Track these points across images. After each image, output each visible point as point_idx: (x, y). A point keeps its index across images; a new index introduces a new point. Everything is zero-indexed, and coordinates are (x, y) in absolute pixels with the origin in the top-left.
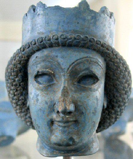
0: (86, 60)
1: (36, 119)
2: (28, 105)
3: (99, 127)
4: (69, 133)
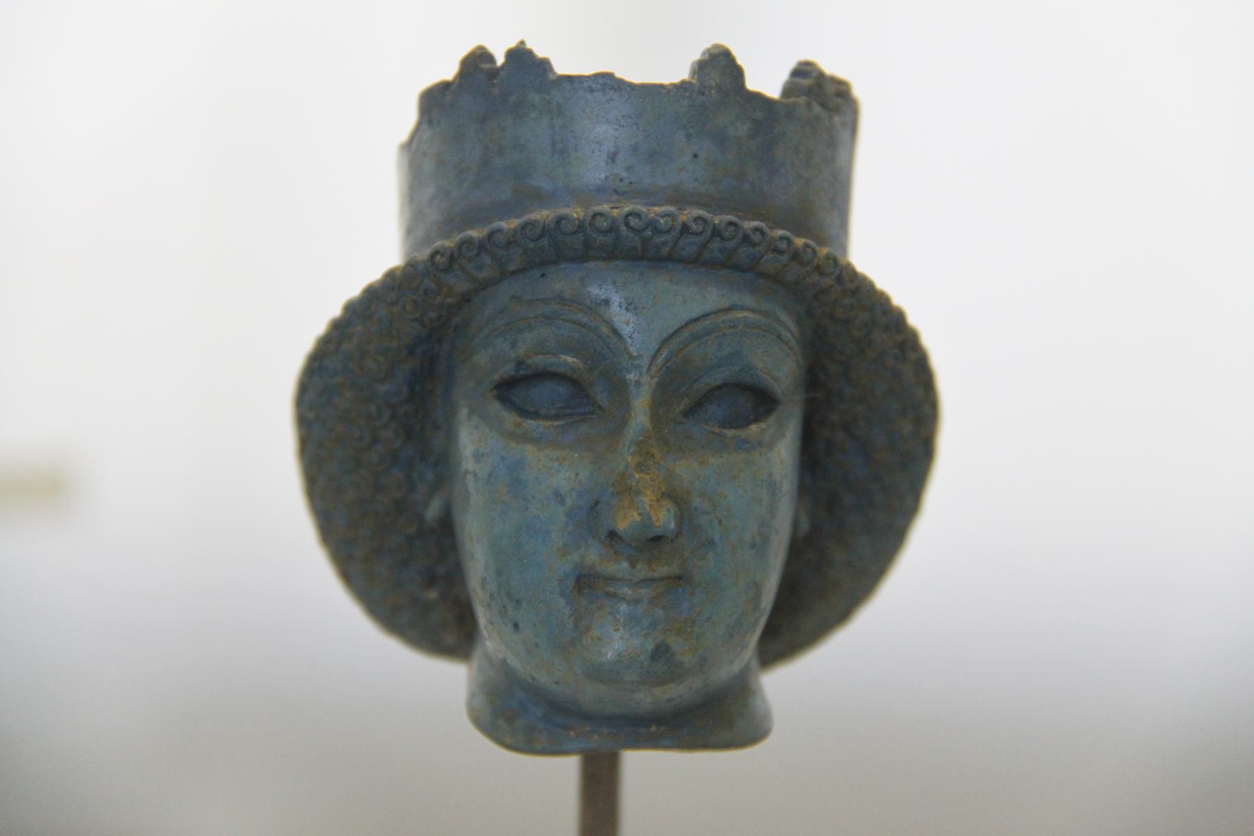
0: (765, 539)
1: (685, 403)
3: (770, 632)
4: (654, 625)
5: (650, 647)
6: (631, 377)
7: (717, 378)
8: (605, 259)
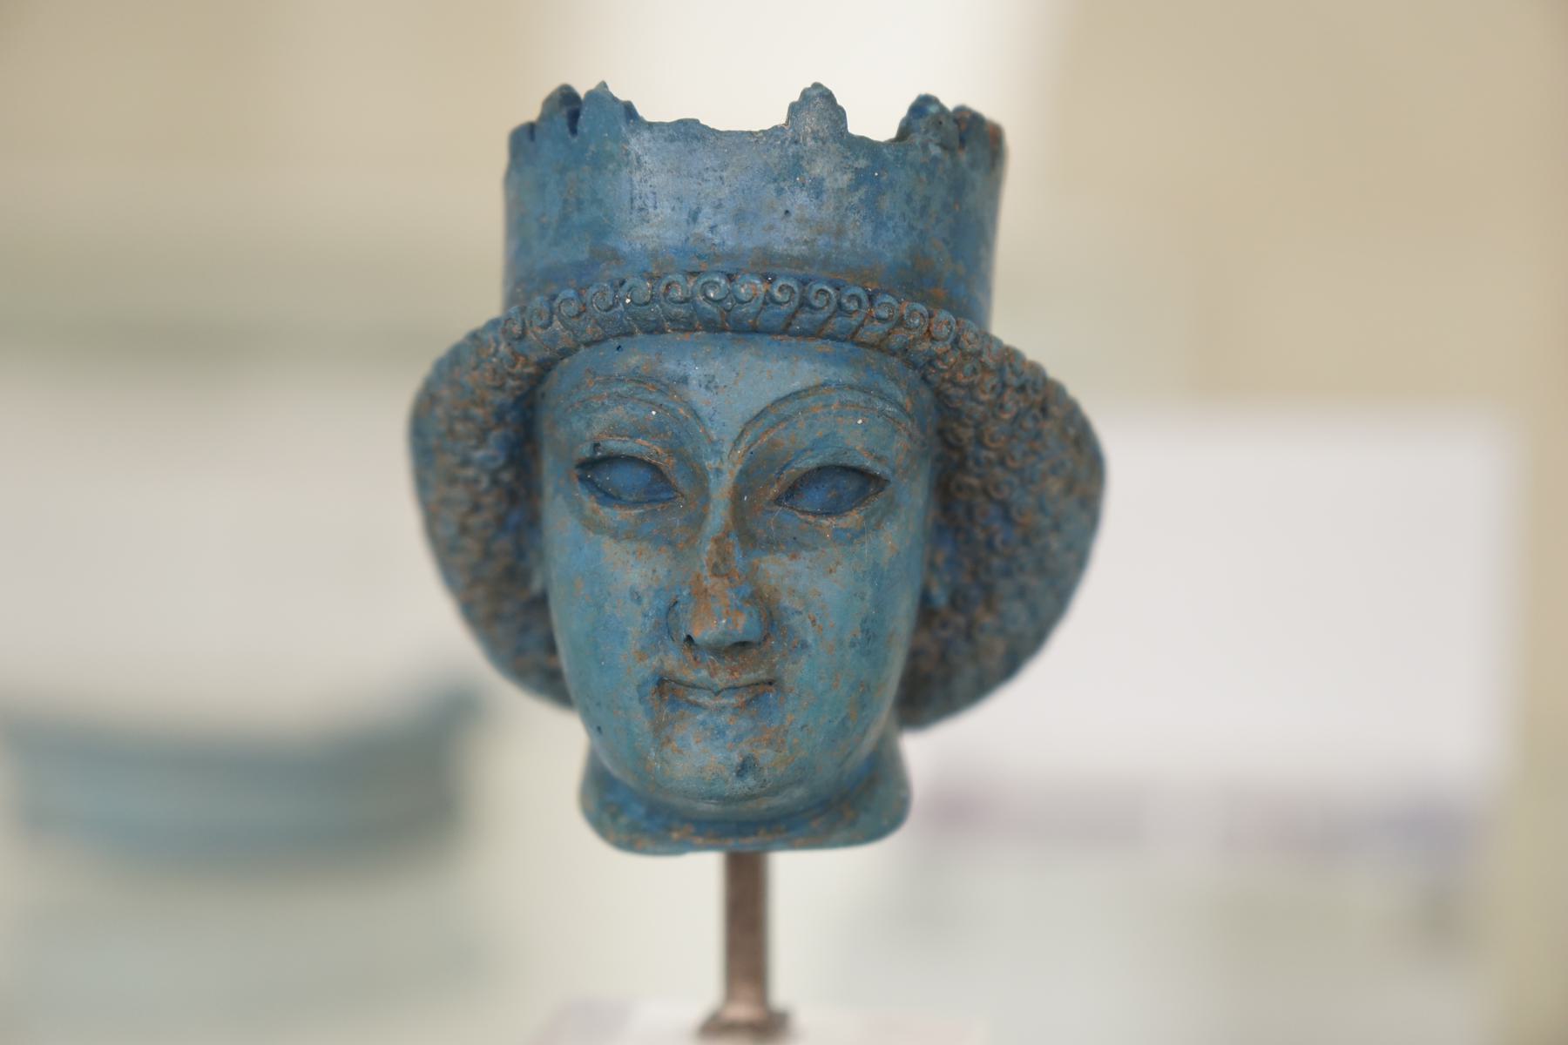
2: (536, 585)
4: (738, 738)
5: (736, 759)
6: (711, 464)
7: (810, 462)
8: (685, 331)
